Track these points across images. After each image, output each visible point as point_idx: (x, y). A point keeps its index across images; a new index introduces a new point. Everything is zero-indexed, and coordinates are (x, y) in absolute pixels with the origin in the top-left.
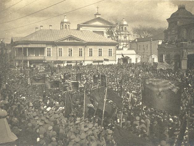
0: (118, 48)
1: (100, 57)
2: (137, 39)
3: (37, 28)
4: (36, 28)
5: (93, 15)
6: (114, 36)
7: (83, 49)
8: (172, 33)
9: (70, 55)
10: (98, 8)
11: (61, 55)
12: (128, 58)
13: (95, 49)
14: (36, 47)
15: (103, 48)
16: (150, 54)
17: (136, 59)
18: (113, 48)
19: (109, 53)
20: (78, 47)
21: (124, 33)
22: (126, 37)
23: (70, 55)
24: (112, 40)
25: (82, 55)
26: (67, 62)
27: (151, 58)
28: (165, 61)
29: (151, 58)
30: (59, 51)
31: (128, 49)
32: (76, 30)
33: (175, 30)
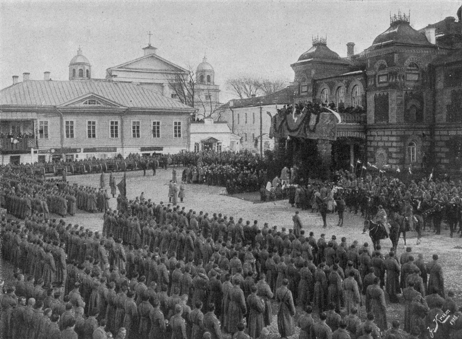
0: (194, 120)
1: (92, 140)
2: (233, 100)
3: (17, 77)
4: (13, 77)
5: (355, 239)
6: (186, 94)
7: (119, 123)
8: (302, 92)
9: (92, 134)
10: (150, 34)
11: (70, 134)
12: (216, 140)
13: (146, 125)
14: (14, 118)
15: (161, 120)
16: (259, 135)
17: (232, 143)
18: (183, 120)
19: (112, 131)
20: (86, 117)
21: (206, 87)
22: (210, 96)
23: (92, 134)
24: (180, 104)
25: (117, 136)
26: (84, 149)
27: (261, 141)
28: (432, 178)
29: (261, 141)
30: (67, 127)
31: (215, 122)
32: (105, 81)
33: (308, 88)
